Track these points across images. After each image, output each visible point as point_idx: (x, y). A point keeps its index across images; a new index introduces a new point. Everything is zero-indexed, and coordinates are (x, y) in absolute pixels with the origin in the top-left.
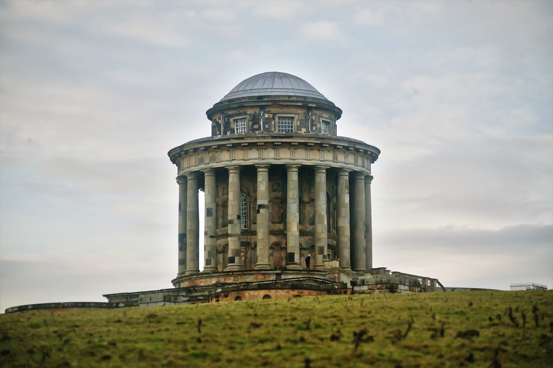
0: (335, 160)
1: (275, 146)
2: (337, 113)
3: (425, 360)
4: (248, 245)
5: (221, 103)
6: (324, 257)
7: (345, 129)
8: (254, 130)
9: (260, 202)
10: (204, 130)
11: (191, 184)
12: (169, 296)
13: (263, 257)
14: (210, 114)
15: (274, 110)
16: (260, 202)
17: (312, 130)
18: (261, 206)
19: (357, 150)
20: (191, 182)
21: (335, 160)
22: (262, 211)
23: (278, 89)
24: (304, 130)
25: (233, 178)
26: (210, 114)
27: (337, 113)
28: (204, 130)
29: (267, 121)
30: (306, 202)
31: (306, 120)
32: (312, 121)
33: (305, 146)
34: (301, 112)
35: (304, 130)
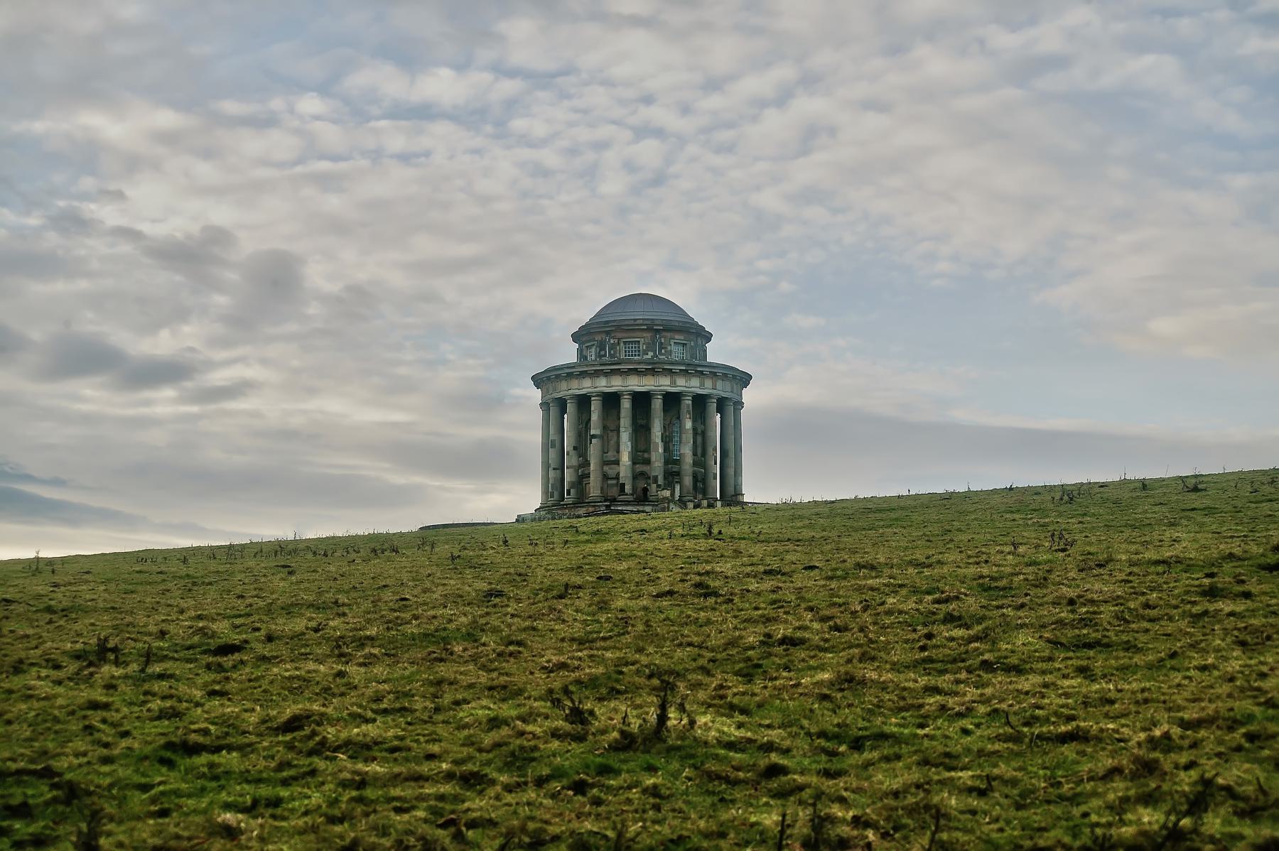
0: (673, 384)
1: (608, 374)
2: (708, 337)
3: (386, 842)
4: (582, 479)
5: (587, 324)
6: (659, 486)
7: (716, 353)
8: (600, 356)
9: (593, 432)
10: (568, 354)
11: (554, 411)
12: (534, 518)
13: (594, 488)
14: (576, 337)
15: (619, 335)
16: (593, 432)
17: (660, 353)
18: (593, 436)
19: (714, 374)
20: (555, 407)
21: (673, 384)
22: (594, 441)
23: (639, 313)
24: (651, 354)
25: (596, 406)
26: (576, 337)
27: (708, 337)
28: (568, 354)
29: (613, 347)
30: (641, 430)
31: (654, 343)
32: (661, 343)
33: (635, 372)
34: (648, 335)
35: (651, 354)
